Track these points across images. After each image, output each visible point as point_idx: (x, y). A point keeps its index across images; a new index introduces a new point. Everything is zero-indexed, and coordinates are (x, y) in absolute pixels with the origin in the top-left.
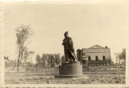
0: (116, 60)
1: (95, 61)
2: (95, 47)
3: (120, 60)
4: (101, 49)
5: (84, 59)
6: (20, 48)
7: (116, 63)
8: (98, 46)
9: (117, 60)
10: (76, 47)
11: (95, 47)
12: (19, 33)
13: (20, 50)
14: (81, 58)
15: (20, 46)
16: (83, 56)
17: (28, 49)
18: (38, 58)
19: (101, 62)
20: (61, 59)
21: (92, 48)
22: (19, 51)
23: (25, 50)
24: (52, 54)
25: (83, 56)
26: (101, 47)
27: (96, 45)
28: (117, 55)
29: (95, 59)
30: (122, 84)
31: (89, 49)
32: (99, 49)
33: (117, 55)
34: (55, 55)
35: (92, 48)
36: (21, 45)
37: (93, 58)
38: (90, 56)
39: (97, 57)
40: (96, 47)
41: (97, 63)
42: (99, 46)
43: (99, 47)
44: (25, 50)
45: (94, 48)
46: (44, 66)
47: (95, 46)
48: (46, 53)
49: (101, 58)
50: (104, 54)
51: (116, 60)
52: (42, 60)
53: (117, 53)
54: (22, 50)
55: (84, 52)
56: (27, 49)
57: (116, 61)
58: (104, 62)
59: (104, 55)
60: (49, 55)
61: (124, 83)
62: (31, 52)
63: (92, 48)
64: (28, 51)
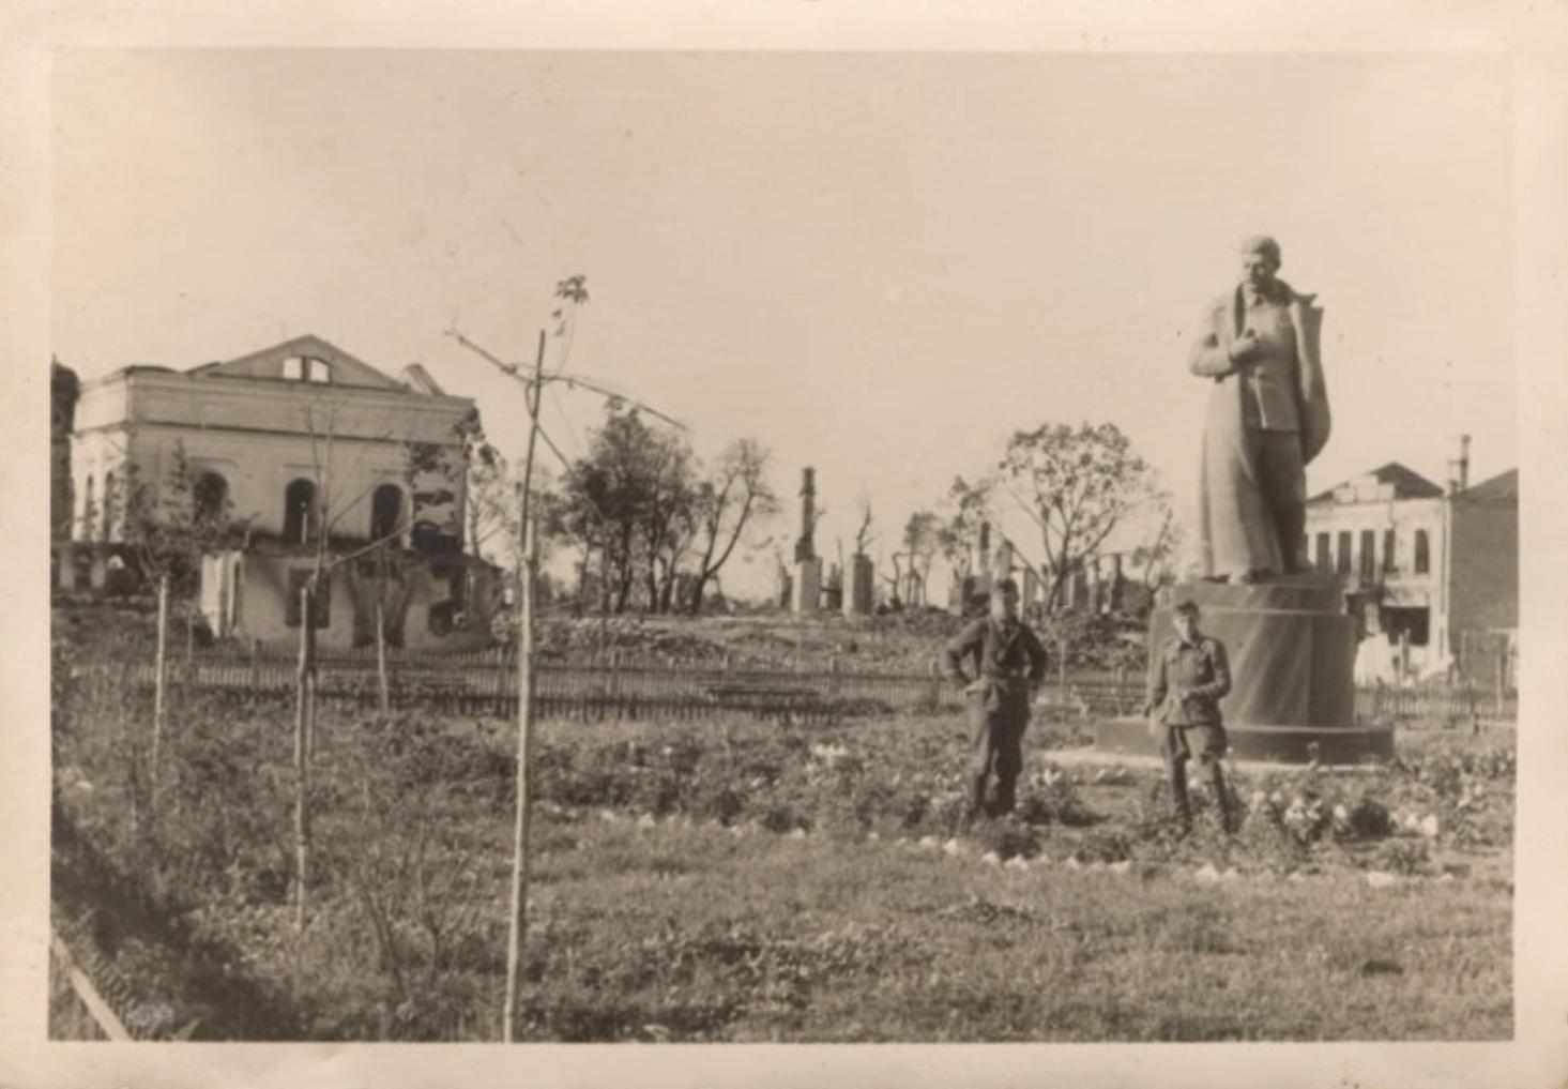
2: (292, 369)
4: (358, 399)
7: (896, 601)
8: (332, 356)
11: (292, 369)
21: (251, 378)
27: (310, 340)
29: (274, 517)
30: (519, 1037)
32: (338, 396)
35: (251, 378)
38: (220, 469)
39: (300, 495)
40: (305, 368)
42: (347, 358)
43: (347, 378)
45: (279, 380)
46: (453, 447)
47: (290, 348)
61: (1498, 1020)
63: (258, 369)
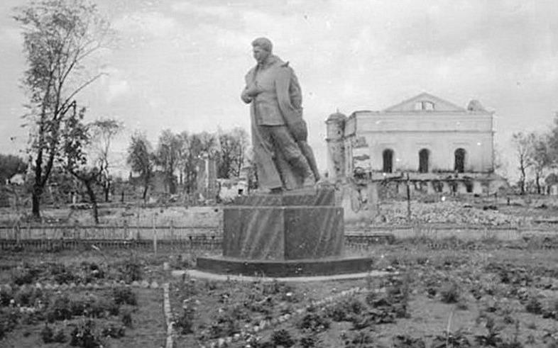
0: (522, 169)
1: (412, 171)
3: (539, 169)
5: (359, 164)
6: (45, 106)
7: (521, 184)
9: (527, 170)
10: (315, 112)
11: (418, 106)
12: (37, 30)
13: (43, 115)
14: (349, 160)
15: (43, 95)
16: (358, 152)
17: (84, 110)
18: (139, 154)
19: (444, 176)
20: (251, 158)
22: (39, 118)
23: (68, 115)
24: (206, 135)
25: (358, 152)
26: (448, 104)
28: (523, 143)
29: (450, 164)
31: (388, 111)
33: (523, 143)
34: (224, 138)
36: (52, 92)
37: (406, 160)
41: (424, 182)
44: (68, 115)
48: (176, 131)
49: (443, 159)
50: (460, 141)
51: (522, 169)
52: (158, 163)
53: (526, 135)
54: (57, 113)
55: (363, 125)
56: (78, 110)
57: (521, 172)
58: (461, 176)
59: (462, 147)
60: (194, 137)
62: (106, 125)
63: (405, 108)
64: (84, 122)
